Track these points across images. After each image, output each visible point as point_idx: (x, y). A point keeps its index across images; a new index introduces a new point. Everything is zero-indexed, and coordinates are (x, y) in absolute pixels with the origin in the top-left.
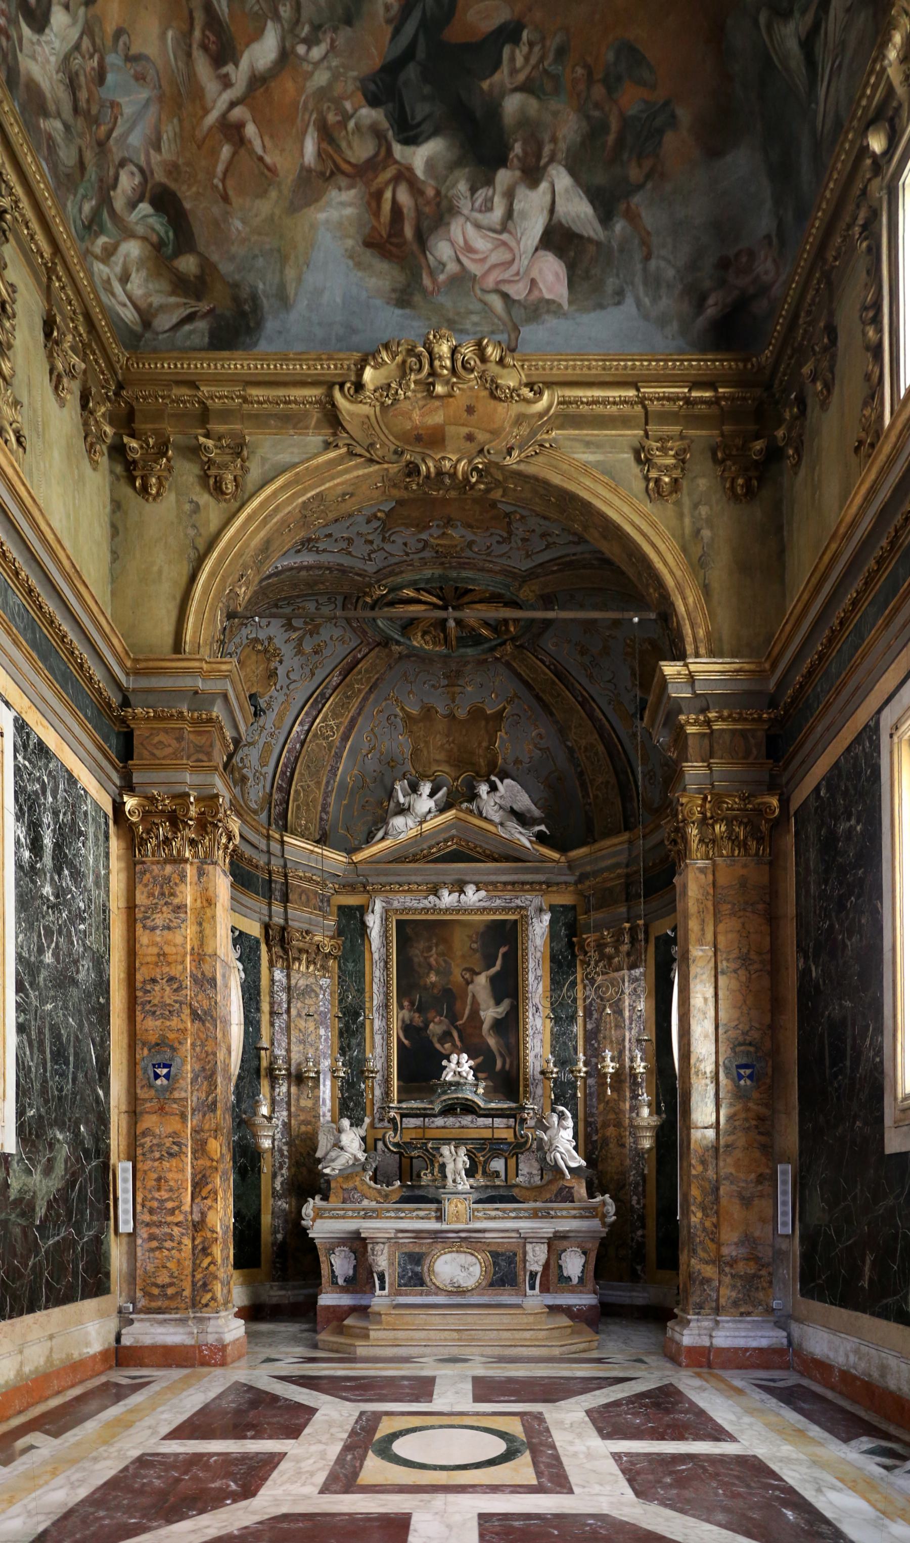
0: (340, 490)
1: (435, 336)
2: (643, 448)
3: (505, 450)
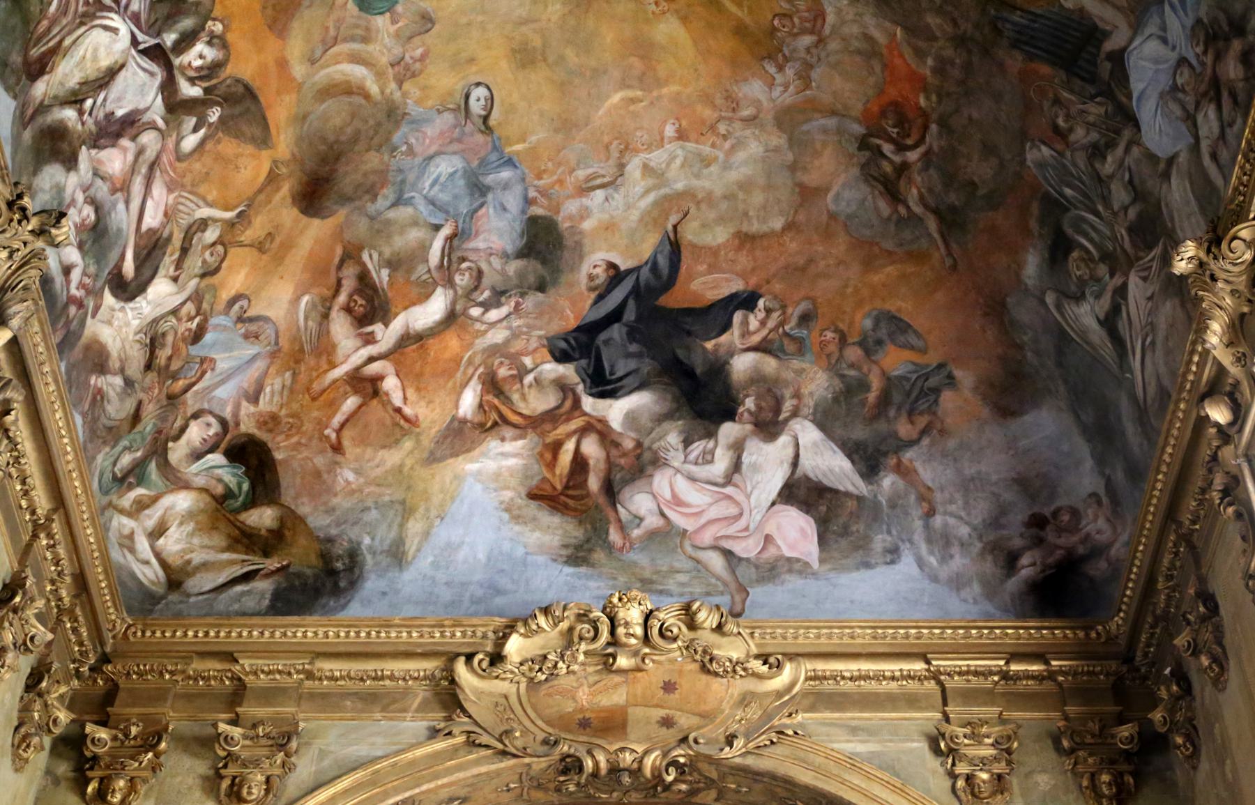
0: (444, 794)
1: (620, 599)
2: (943, 735)
3: (722, 739)
